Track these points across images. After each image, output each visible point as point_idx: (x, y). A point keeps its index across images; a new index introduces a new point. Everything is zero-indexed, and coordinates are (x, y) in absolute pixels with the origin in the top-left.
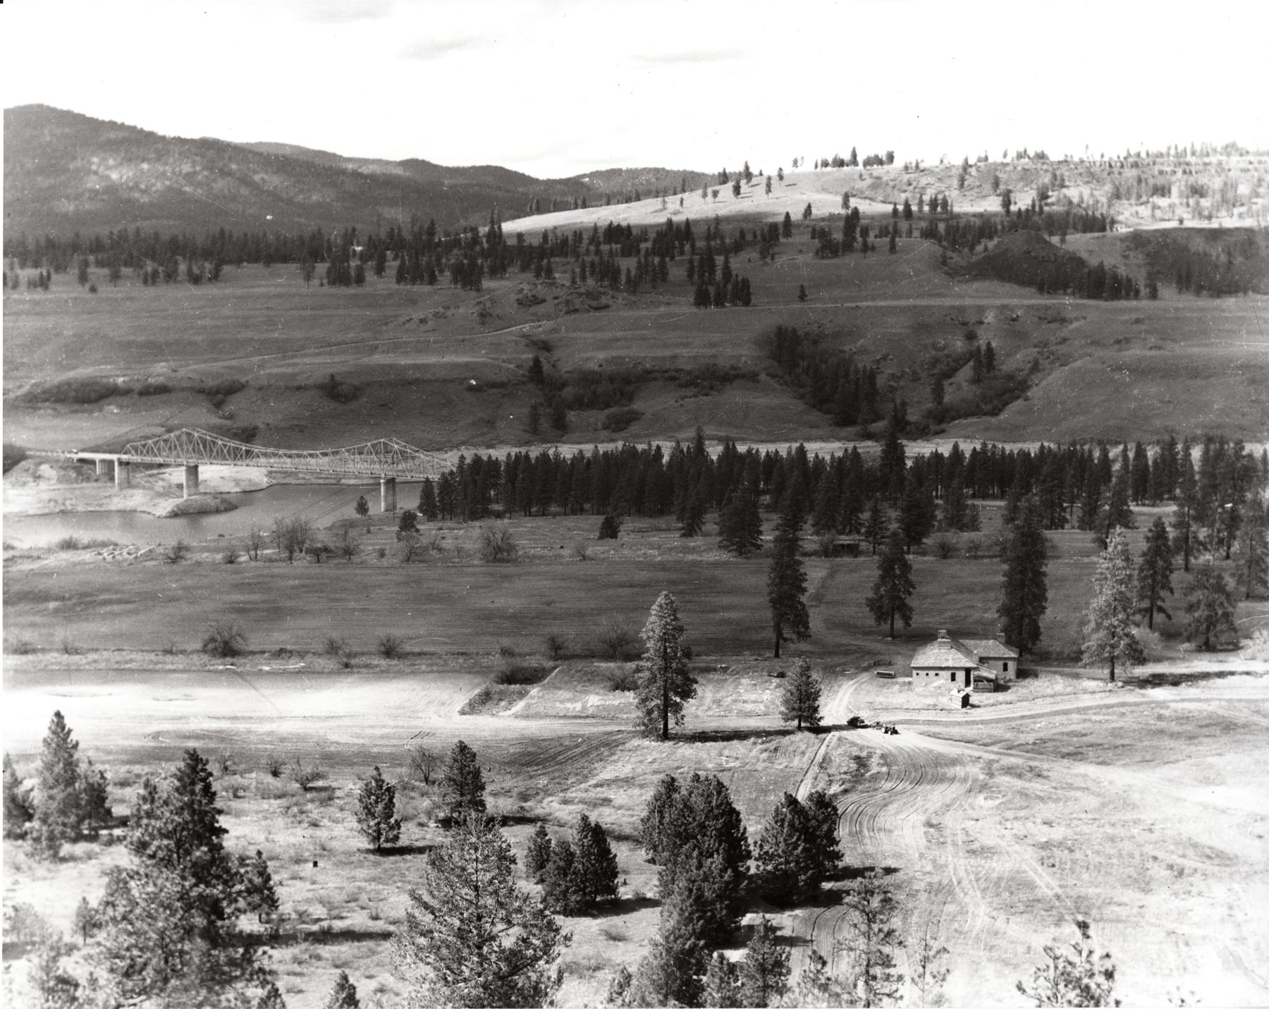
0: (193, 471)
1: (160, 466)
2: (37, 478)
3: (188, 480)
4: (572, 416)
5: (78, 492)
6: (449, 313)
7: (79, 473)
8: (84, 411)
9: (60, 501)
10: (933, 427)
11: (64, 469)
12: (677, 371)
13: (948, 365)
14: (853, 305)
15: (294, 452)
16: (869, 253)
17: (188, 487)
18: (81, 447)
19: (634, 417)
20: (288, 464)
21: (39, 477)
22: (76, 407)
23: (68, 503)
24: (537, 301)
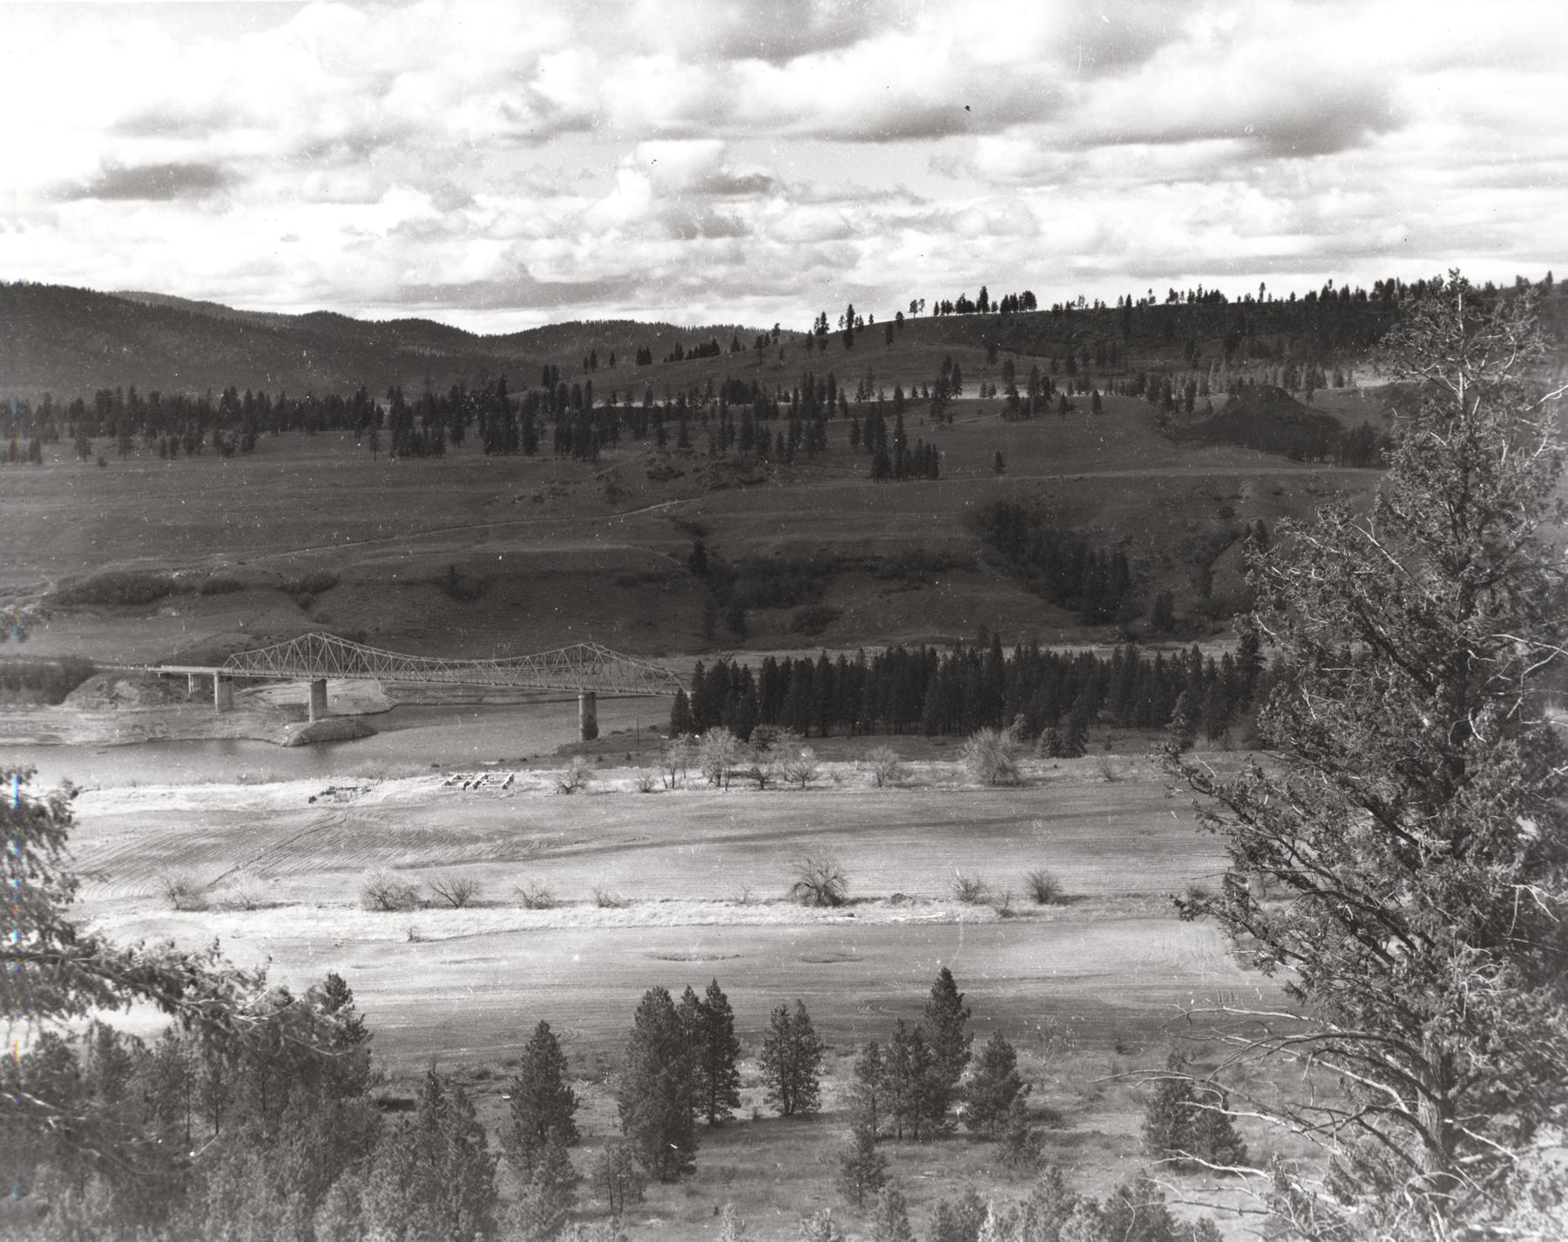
0: (320, 688)
1: (256, 681)
2: (115, 698)
3: (314, 698)
4: (752, 616)
5: (167, 715)
6: (569, 489)
7: (168, 692)
8: (134, 615)
9: (147, 728)
10: (1211, 625)
11: (148, 686)
12: (875, 559)
13: (1204, 549)
14: (1077, 476)
15: (456, 661)
16: (1068, 415)
17: (315, 707)
18: (155, 659)
19: (829, 617)
20: (417, 679)
21: (117, 696)
22: (123, 608)
23: (158, 729)
24: (672, 474)
